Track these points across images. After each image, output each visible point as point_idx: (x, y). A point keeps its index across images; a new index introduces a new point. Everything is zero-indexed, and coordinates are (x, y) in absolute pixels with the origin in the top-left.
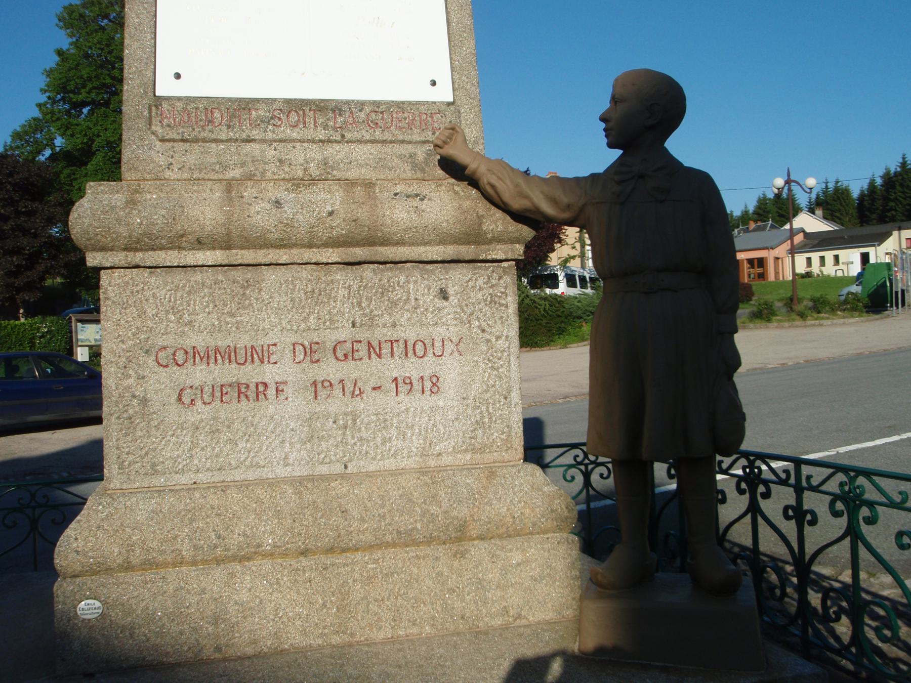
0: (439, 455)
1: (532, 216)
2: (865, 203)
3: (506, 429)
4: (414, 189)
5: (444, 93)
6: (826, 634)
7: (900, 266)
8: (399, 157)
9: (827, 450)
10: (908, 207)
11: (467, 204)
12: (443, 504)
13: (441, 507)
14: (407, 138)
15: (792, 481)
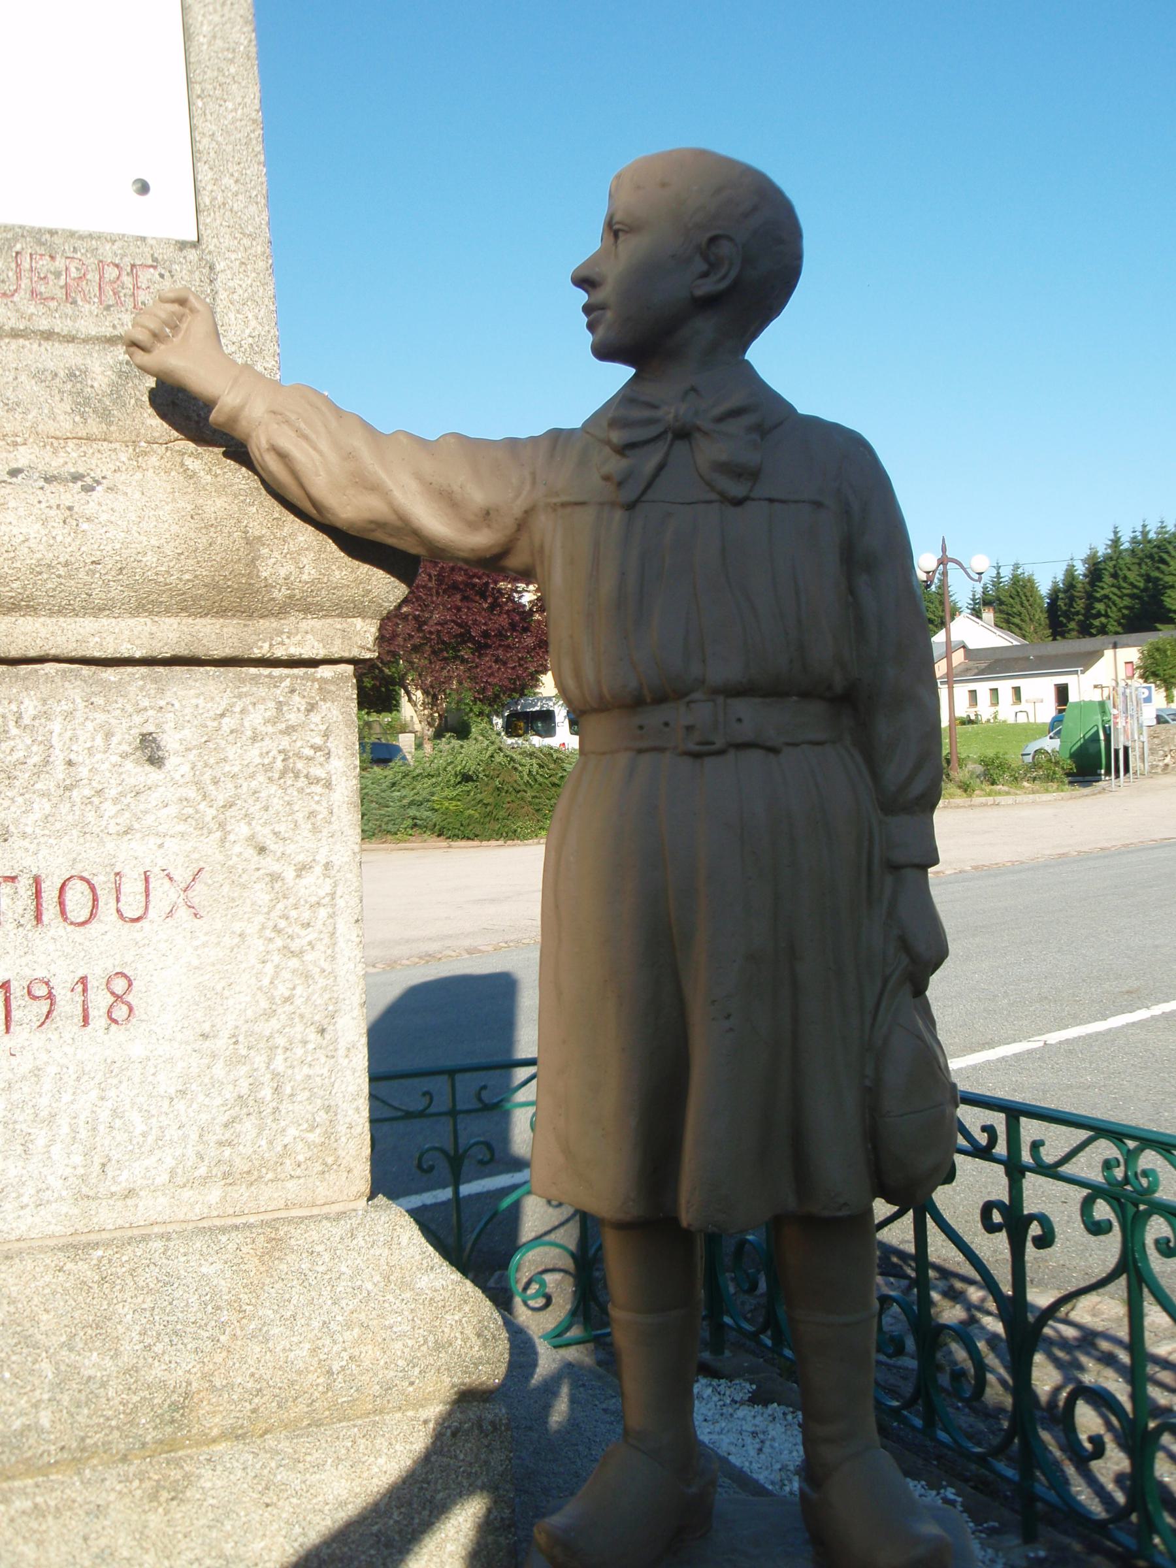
0: (130, 1193)
1: (391, 541)
2: (1060, 603)
3: (322, 1117)
4: (68, 459)
5: (169, 217)
6: (1058, 1453)
7: (1121, 707)
8: (38, 375)
9: (1027, 1038)
10: (1126, 612)
11: (216, 506)
12: (125, 1347)
13: (117, 1355)
14: (60, 326)
15: (1001, 1149)
